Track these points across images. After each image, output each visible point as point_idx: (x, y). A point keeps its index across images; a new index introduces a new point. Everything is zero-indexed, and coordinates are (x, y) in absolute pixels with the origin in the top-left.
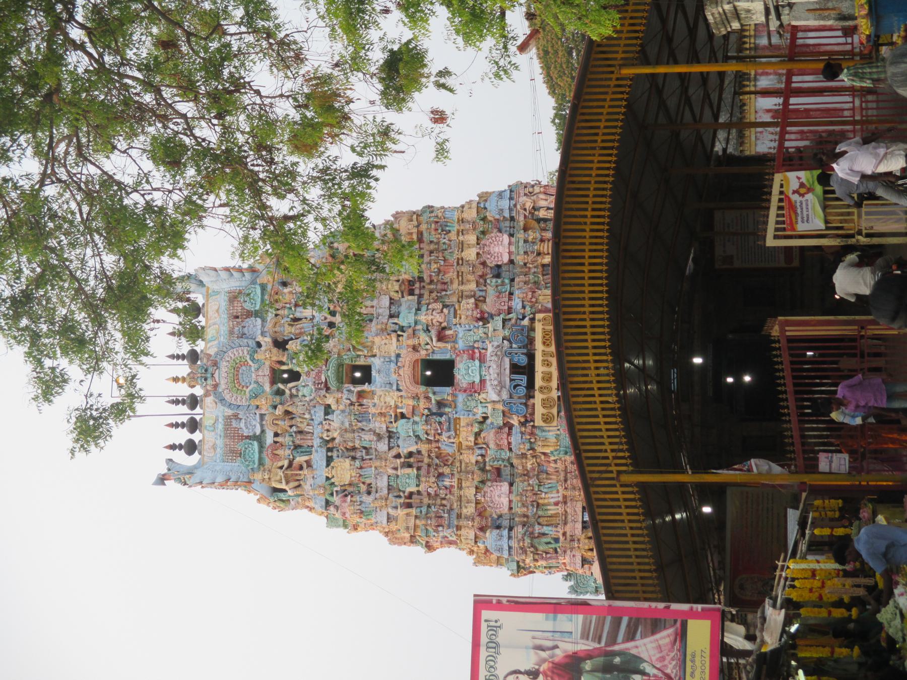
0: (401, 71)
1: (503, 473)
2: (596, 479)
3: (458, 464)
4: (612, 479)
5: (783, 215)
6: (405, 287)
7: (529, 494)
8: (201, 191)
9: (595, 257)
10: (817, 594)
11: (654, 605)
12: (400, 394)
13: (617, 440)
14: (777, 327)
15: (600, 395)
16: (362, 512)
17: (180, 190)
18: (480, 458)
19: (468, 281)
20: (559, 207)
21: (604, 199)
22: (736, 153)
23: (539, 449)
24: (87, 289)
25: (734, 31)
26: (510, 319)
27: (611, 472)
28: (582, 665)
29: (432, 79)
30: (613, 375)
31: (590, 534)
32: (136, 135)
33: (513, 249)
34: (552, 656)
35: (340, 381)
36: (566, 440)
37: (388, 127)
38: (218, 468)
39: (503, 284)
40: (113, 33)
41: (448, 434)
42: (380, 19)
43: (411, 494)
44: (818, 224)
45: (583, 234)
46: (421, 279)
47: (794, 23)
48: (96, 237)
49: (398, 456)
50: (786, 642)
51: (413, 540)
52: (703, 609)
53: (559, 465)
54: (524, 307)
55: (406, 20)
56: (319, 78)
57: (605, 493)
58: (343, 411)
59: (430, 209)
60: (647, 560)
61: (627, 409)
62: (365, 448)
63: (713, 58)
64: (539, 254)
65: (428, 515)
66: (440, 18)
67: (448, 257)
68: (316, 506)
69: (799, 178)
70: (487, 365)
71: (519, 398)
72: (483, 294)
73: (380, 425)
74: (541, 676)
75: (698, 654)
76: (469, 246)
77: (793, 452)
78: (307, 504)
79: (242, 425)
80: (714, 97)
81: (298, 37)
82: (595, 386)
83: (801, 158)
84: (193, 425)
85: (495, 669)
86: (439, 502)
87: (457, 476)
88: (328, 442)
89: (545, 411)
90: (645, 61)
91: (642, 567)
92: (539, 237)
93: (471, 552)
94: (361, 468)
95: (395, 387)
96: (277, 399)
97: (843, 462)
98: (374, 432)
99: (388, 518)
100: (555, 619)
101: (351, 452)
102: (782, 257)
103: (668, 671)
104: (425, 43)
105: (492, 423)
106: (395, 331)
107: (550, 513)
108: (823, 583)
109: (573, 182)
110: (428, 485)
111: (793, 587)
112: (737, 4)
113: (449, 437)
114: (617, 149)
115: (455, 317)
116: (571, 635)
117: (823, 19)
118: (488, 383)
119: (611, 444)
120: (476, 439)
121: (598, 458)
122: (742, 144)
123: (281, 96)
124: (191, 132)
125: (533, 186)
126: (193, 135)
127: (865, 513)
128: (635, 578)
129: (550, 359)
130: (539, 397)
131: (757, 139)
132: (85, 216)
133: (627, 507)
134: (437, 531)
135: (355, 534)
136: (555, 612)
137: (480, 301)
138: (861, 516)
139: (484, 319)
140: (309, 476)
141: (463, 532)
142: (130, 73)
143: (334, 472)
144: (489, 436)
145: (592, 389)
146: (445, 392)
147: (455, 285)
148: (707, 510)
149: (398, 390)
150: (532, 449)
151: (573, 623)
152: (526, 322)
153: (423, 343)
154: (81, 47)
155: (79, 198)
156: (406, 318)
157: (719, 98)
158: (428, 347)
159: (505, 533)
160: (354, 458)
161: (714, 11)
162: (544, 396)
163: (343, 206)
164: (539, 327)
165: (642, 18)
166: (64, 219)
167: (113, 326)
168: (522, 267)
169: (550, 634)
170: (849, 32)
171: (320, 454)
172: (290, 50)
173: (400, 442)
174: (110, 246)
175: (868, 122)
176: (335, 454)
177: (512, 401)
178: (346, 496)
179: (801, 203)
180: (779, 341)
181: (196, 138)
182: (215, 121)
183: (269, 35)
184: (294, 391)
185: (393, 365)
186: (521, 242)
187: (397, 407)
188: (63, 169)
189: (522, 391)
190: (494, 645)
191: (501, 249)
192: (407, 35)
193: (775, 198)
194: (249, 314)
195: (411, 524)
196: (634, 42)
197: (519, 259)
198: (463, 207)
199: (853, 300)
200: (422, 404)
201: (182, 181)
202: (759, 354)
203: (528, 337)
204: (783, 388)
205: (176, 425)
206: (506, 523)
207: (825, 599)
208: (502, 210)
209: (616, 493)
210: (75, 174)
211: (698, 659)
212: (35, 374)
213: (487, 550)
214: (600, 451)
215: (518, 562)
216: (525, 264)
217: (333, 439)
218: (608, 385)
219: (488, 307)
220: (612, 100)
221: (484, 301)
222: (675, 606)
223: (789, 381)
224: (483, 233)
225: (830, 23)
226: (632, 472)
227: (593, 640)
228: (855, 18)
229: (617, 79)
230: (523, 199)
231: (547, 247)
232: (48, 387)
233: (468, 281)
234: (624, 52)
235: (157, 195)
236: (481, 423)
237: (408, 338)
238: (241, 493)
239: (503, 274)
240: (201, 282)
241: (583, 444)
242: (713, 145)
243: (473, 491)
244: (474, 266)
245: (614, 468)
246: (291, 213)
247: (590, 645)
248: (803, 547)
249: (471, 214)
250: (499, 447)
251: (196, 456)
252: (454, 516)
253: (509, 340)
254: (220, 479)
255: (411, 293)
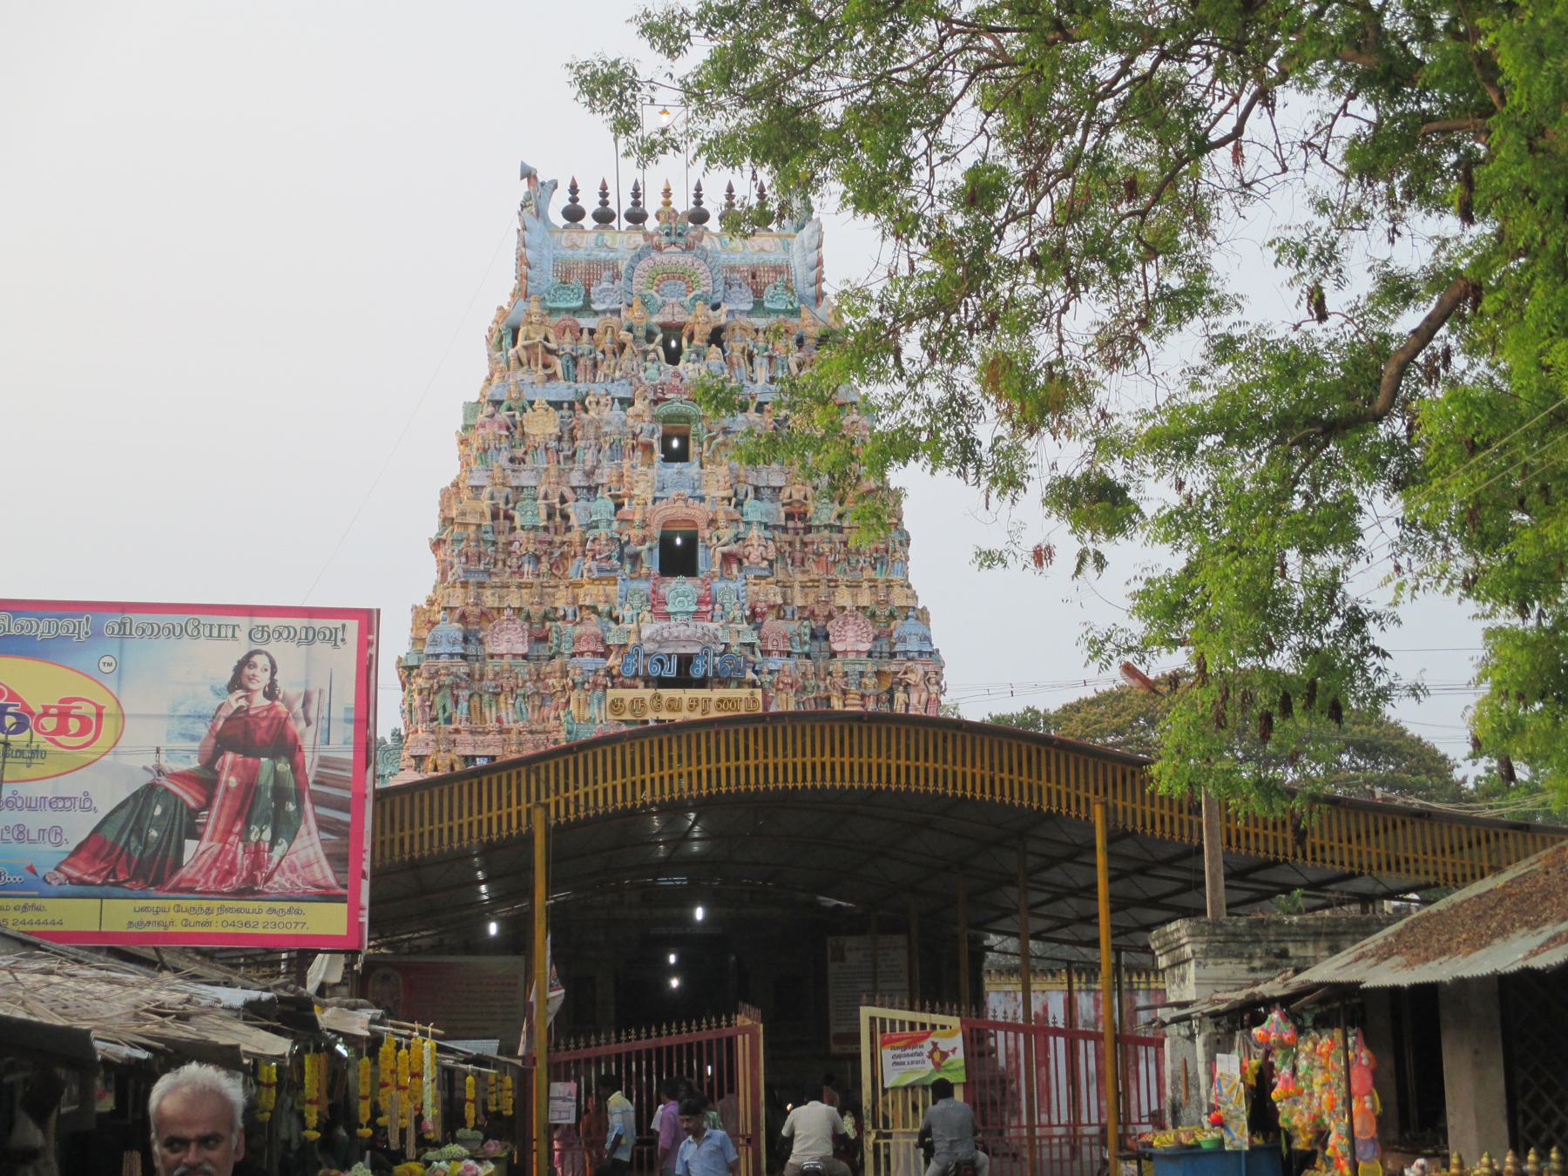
0: (1097, 504)
1: (540, 646)
2: (538, 775)
3: (552, 583)
4: (538, 797)
5: (902, 1029)
6: (796, 508)
7: (512, 682)
8: (933, 235)
9: (842, 771)
10: (388, 1079)
11: (367, 856)
12: (650, 502)
13: (591, 803)
14: (748, 1022)
15: (652, 780)
16: (485, 451)
17: (932, 205)
18: (561, 613)
19: (806, 595)
20: (907, 720)
21: (922, 782)
22: (986, 965)
23: (574, 695)
24: (796, 80)
25: (1155, 959)
26: (753, 653)
27: (548, 796)
28: (284, 759)
29: (1091, 546)
30: (681, 797)
31: (457, 768)
32: (1006, 141)
33: (851, 657)
34: (296, 718)
35: (667, 419)
36: (587, 734)
37: (1021, 485)
38: (545, 252)
39: (803, 643)
40: (1146, 115)
41: (594, 568)
42: (1169, 479)
43: (511, 519)
44: (892, 1078)
45: (874, 754)
46: (808, 530)
47: (1167, 1042)
48: (868, 92)
49: (563, 500)
50: (326, 1038)
51: (447, 521)
52: (361, 924)
53: (553, 723)
54: (771, 672)
55: (1166, 511)
56: (1084, 388)
57: (519, 787)
58: (625, 423)
59: (906, 542)
60: (426, 846)
61: (631, 817)
62: (574, 454)
63: (1117, 931)
64: (844, 692)
65: (485, 541)
66: (1170, 560)
67: (839, 567)
68: (493, 388)
69: (954, 1051)
70: (691, 623)
71: (645, 667)
72: (789, 616)
73: (605, 475)
74: (268, 702)
75: (301, 918)
76: (854, 596)
77: (577, 1047)
78: (497, 375)
79: (605, 285)
80: (1064, 934)
81: (1141, 361)
82: (666, 773)
83: (981, 1055)
84: (604, 217)
85: (278, 640)
86: (501, 556)
87: (536, 581)
88: (582, 402)
89: (627, 702)
90: (1112, 838)
91: (417, 839)
92: (868, 692)
93: (431, 602)
94: (547, 449)
95: (658, 494)
96: (641, 333)
97: (564, 1115)
98: (595, 467)
99: (477, 487)
100: (347, 720)
101: (568, 435)
102: (844, 1029)
103: (276, 877)
104: (1139, 537)
105: (609, 630)
106: (736, 494)
107: (486, 711)
108: (404, 1088)
109: (945, 740)
110: (523, 542)
111: (398, 1047)
112: (1193, 963)
113: (590, 570)
114: (992, 800)
115: (756, 577)
116: (326, 743)
117: (1174, 1082)
118: (665, 624)
119: (586, 794)
120: (588, 607)
121: (567, 777)
122: (1000, 972)
123: (1061, 341)
124: (1013, 220)
125: (938, 683)
126: (1007, 222)
127: (494, 1147)
128: (402, 830)
129: (699, 709)
130: (647, 694)
131: (1007, 993)
132: (894, 75)
133: (500, 818)
134: (460, 554)
135: (455, 440)
136: (357, 721)
137: (779, 611)
138: (490, 1141)
139: (754, 617)
140: (534, 377)
141: (459, 591)
142: (1090, 136)
143: (540, 411)
144: (592, 626)
145: (661, 769)
146: (652, 564)
147: (800, 577)
148: (493, 929)
149: (655, 500)
150: (575, 686)
151: (342, 746)
152: (750, 675)
153: (719, 532)
154: (1125, 71)
155: (920, 67)
156: (754, 510)
157: (1063, 934)
158: (715, 540)
159: (458, 649)
160: (560, 439)
161: (1183, 932)
162: (647, 702)
163: (920, 430)
164: (744, 693)
165: (1172, 833)
166: (891, 49)
167: (748, 116)
168: (826, 669)
169: (325, 713)
170: (1157, 1120)
171: (565, 392)
172: (1124, 350)
173: (582, 503)
174: (856, 109)
175: (1032, 1151)
176: (565, 412)
177: (641, 658)
178: (508, 429)
179: (920, 1054)
180: (729, 1025)
181: (1004, 226)
182: (1027, 253)
183: (1144, 324)
184: (652, 355)
185: (688, 492)
186: (861, 668)
187: (631, 497)
188: (958, 45)
189: (655, 671)
190: (310, 638)
191: (850, 640)
192: (1149, 509)
193: (925, 1017)
194: (758, 293)
195: (469, 519)
196: (1139, 823)
197: (837, 666)
198: (909, 587)
199: (784, 1132)
200: (636, 533)
201: (945, 208)
202: (711, 996)
203: (730, 678)
204: (664, 1032)
205: (604, 194)
206: (472, 650)
207: (382, 1091)
208: (904, 641)
209: (519, 803)
210: (953, 61)
211: (293, 918)
212: (678, 12)
213: (434, 624)
214: (576, 780)
215: (418, 667)
216: (830, 674)
217: (586, 411)
218: (667, 790)
219: (770, 621)
220: (1059, 792)
221: (778, 618)
222: (365, 885)
223: (675, 1040)
224: (873, 615)
225: (1168, 1092)
226: (547, 825)
227: (318, 774)
228: (1175, 1127)
229: (1087, 799)
230: (920, 669)
231: (854, 707)
232: (662, 30)
233: (806, 595)
234: (1125, 809)
235: (925, 174)
236: (610, 614)
237: (726, 513)
238: (511, 283)
239: (816, 643)
240: (803, 227)
241: (586, 758)
242: (997, 932)
243: (516, 605)
244: (827, 603)
245: (552, 799)
246: (903, 358)
247: (311, 770)
248: (449, 1061)
249: (898, 599)
250: (577, 640)
251: (561, 222)
252: (481, 579)
253: (724, 652)
254: (530, 254)
255: (789, 516)
